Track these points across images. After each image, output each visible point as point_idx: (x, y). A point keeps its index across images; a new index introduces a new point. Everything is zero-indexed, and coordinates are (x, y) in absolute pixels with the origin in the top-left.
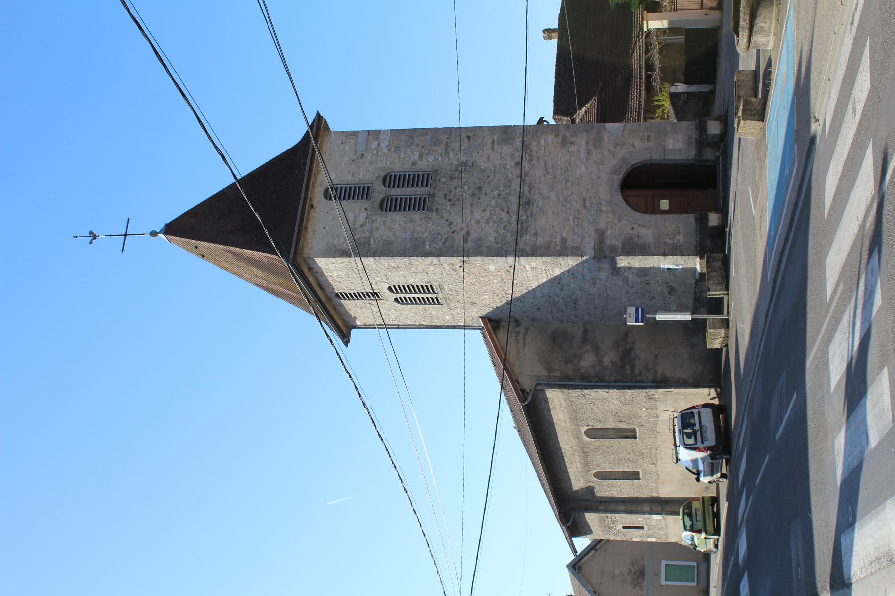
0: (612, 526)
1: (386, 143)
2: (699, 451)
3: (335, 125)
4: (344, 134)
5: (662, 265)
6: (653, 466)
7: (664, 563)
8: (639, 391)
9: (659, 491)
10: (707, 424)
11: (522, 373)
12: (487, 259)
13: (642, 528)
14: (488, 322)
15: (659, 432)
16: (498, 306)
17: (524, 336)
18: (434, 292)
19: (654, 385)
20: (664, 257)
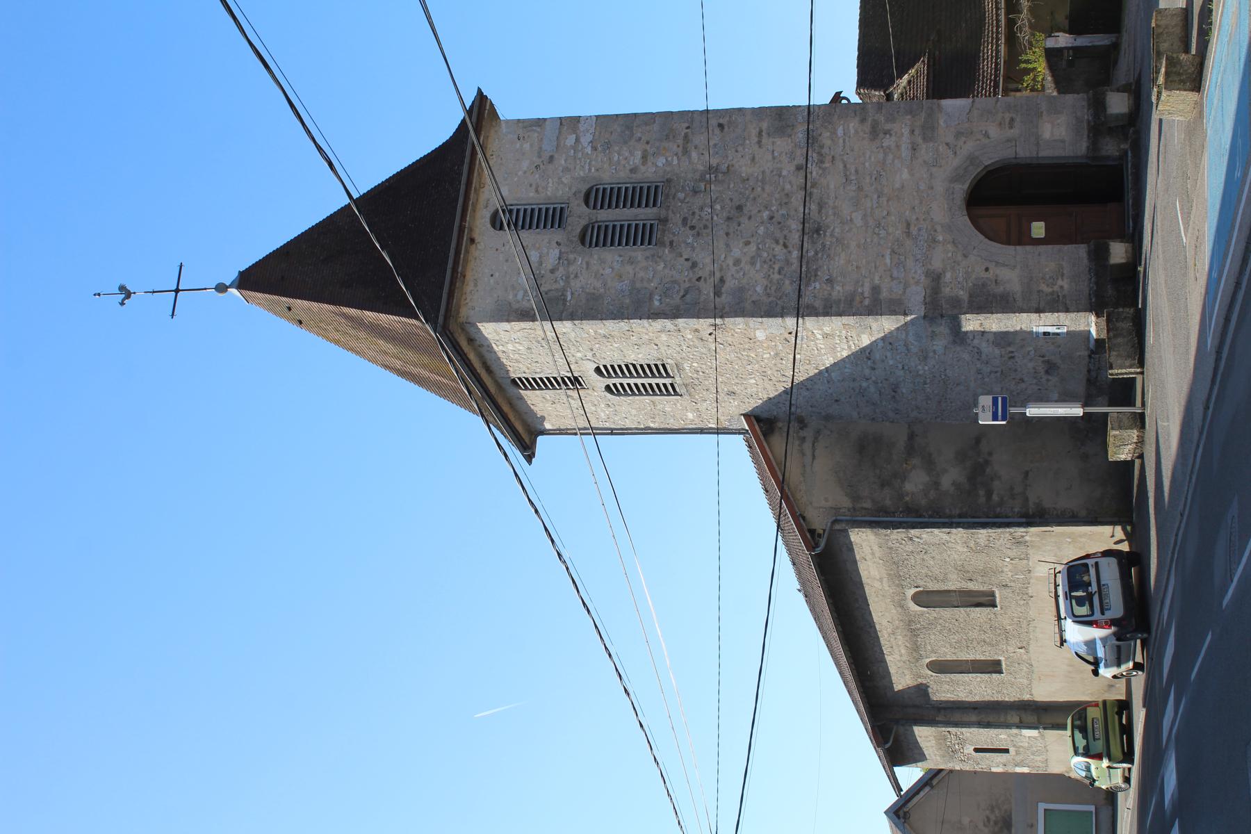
0: (957, 747)
2: (1097, 627)
3: (508, 109)
5: (1034, 327)
6: (1022, 651)
7: (1042, 807)
8: (999, 530)
9: (1033, 691)
10: (1110, 583)
11: (811, 503)
13: (1006, 751)
14: (755, 423)
15: (1032, 597)
17: (813, 445)
18: (668, 376)
19: (1024, 520)
20: (1038, 314)
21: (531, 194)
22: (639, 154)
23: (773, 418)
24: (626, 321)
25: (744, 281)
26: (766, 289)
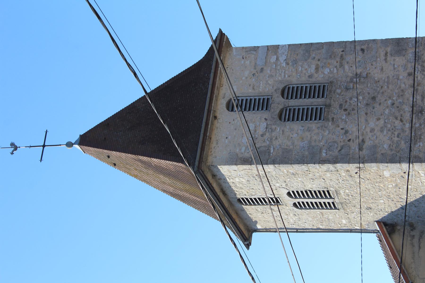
1: (284, 57)
4: (244, 50)
11: (418, 276)
12: (382, 166)
14: (383, 226)
16: (393, 210)
17: (419, 240)
23: (394, 223)
24: (306, 165)
25: (377, 142)
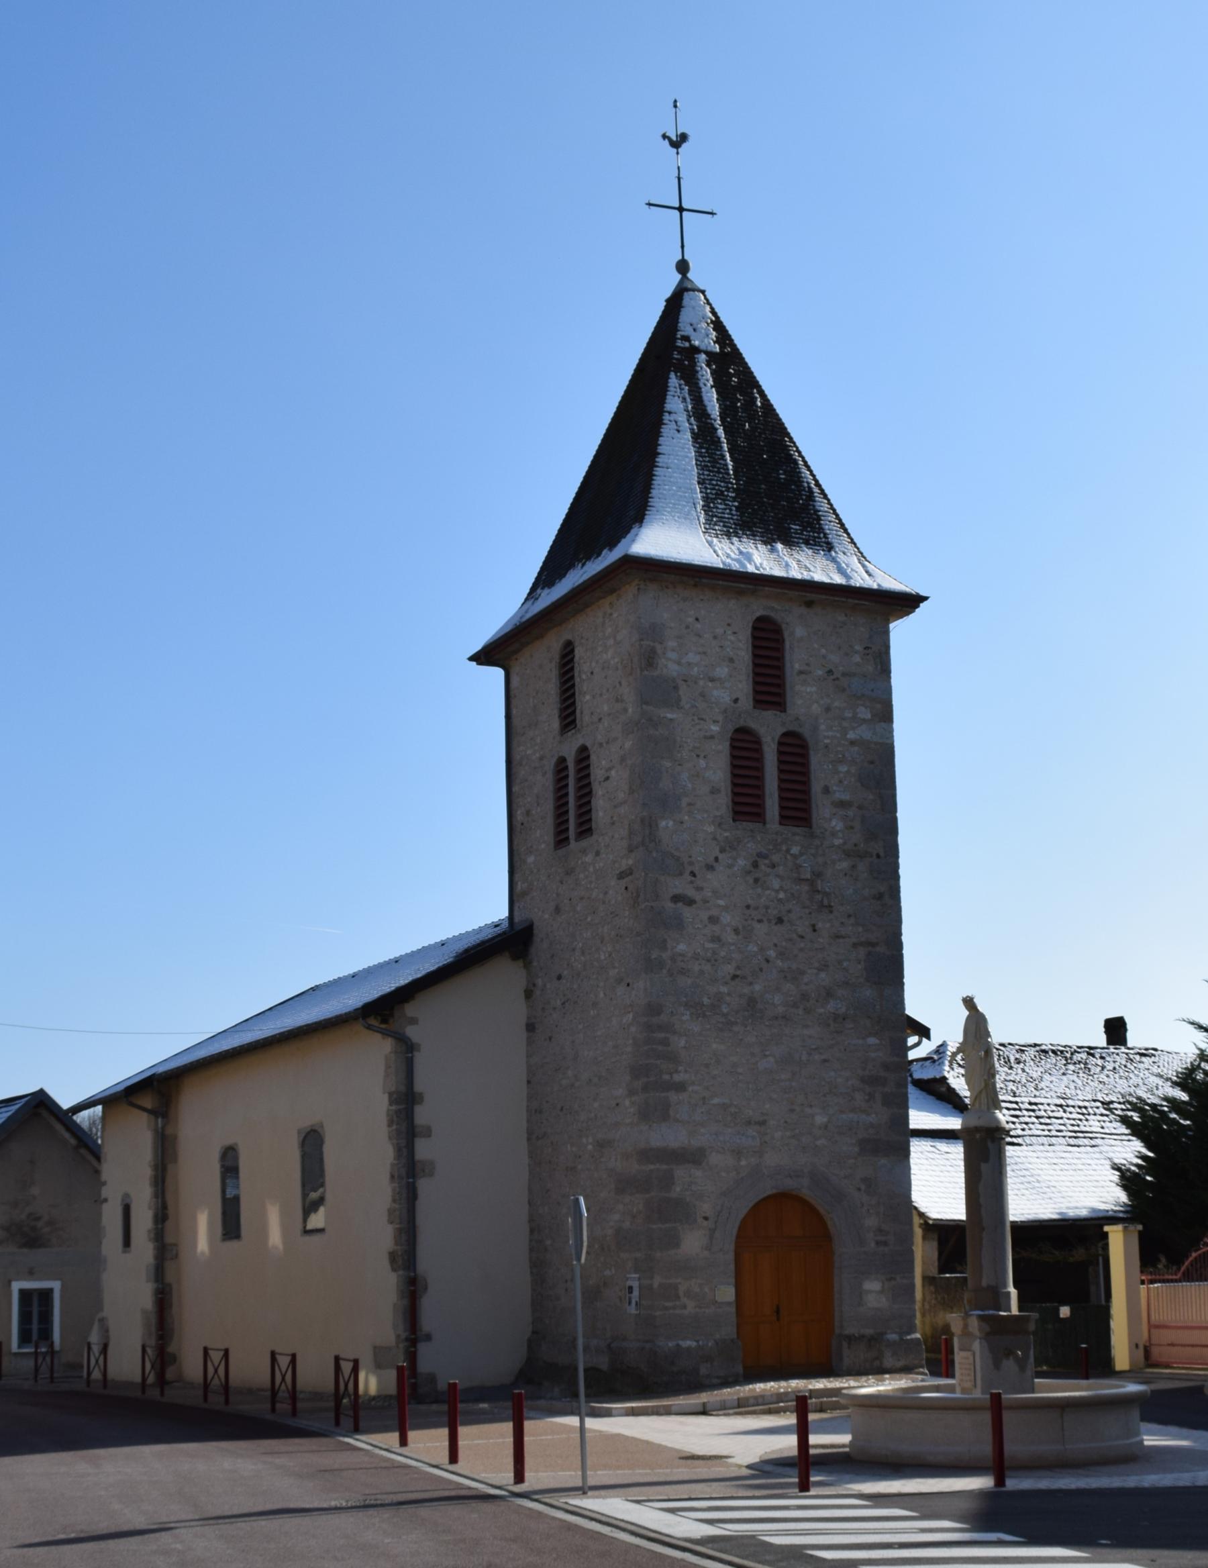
7: (56, 1285)
21: (797, 666)
22: (846, 797)
26: (681, 955)
